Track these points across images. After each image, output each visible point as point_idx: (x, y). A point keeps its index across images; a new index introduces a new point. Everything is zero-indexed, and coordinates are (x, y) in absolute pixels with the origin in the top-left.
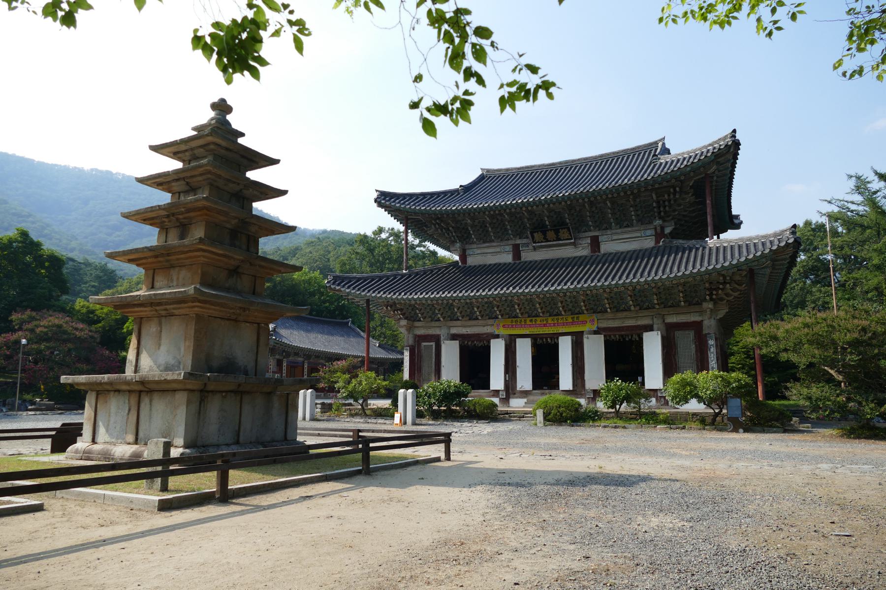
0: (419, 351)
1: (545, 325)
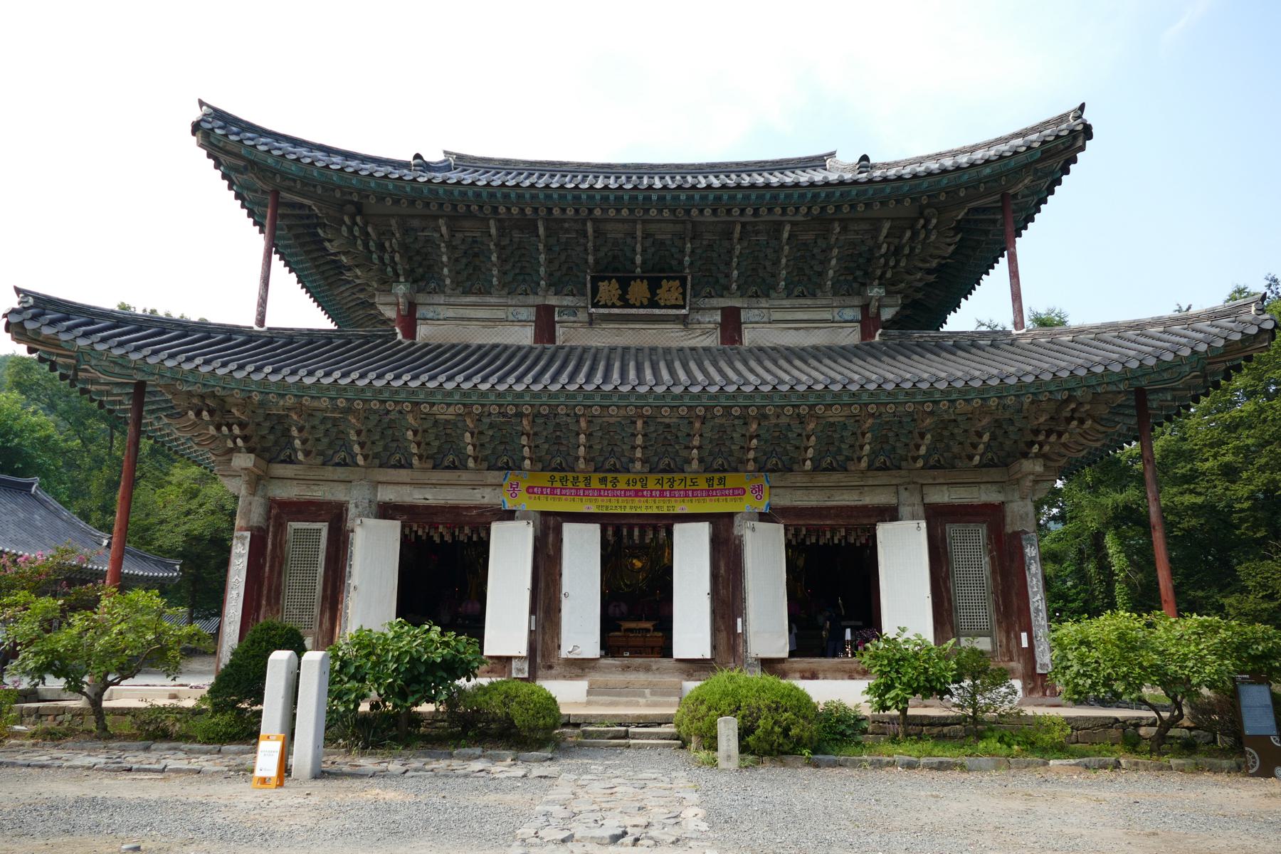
0: (279, 545)
1: (637, 494)
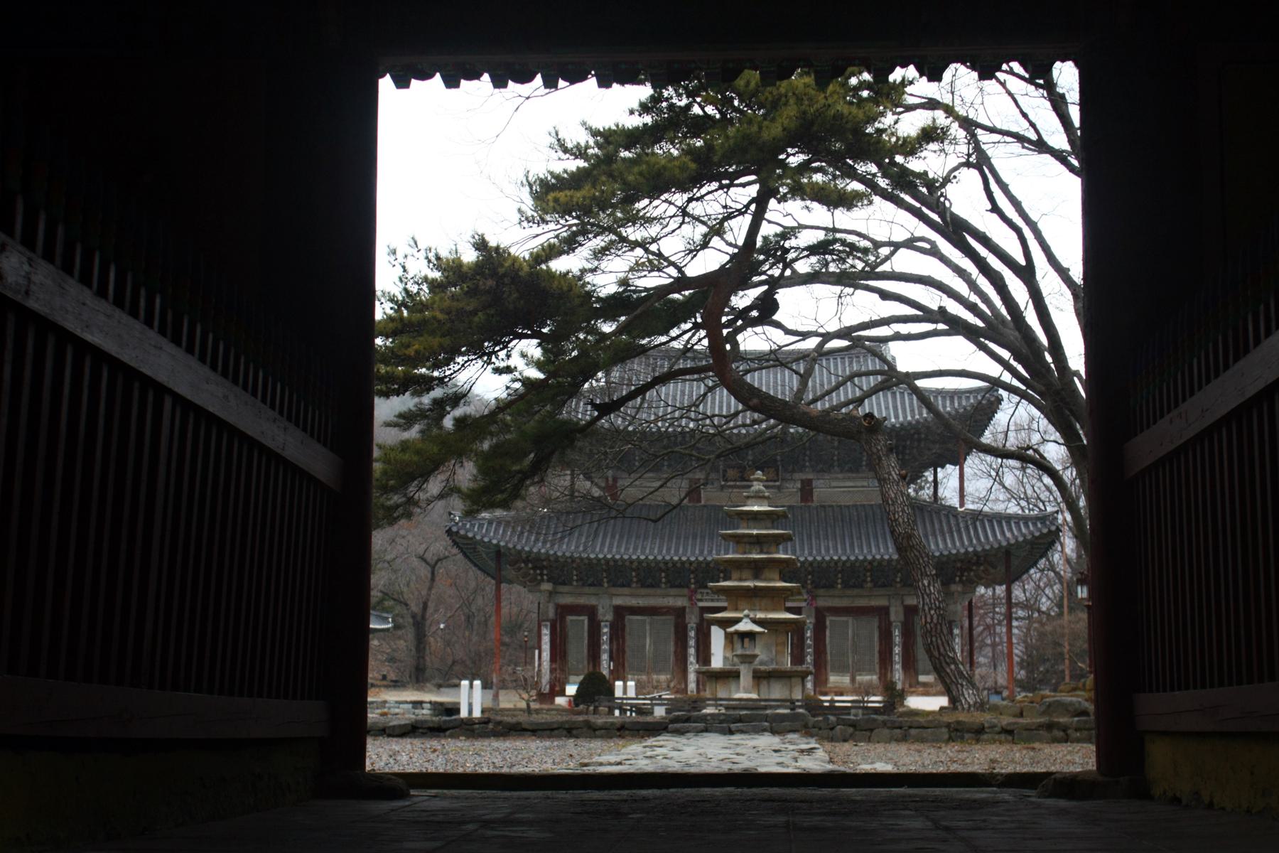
0: (563, 628)
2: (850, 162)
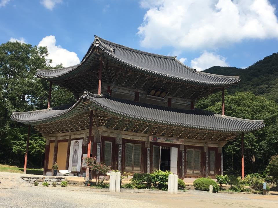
2: (134, 85)
